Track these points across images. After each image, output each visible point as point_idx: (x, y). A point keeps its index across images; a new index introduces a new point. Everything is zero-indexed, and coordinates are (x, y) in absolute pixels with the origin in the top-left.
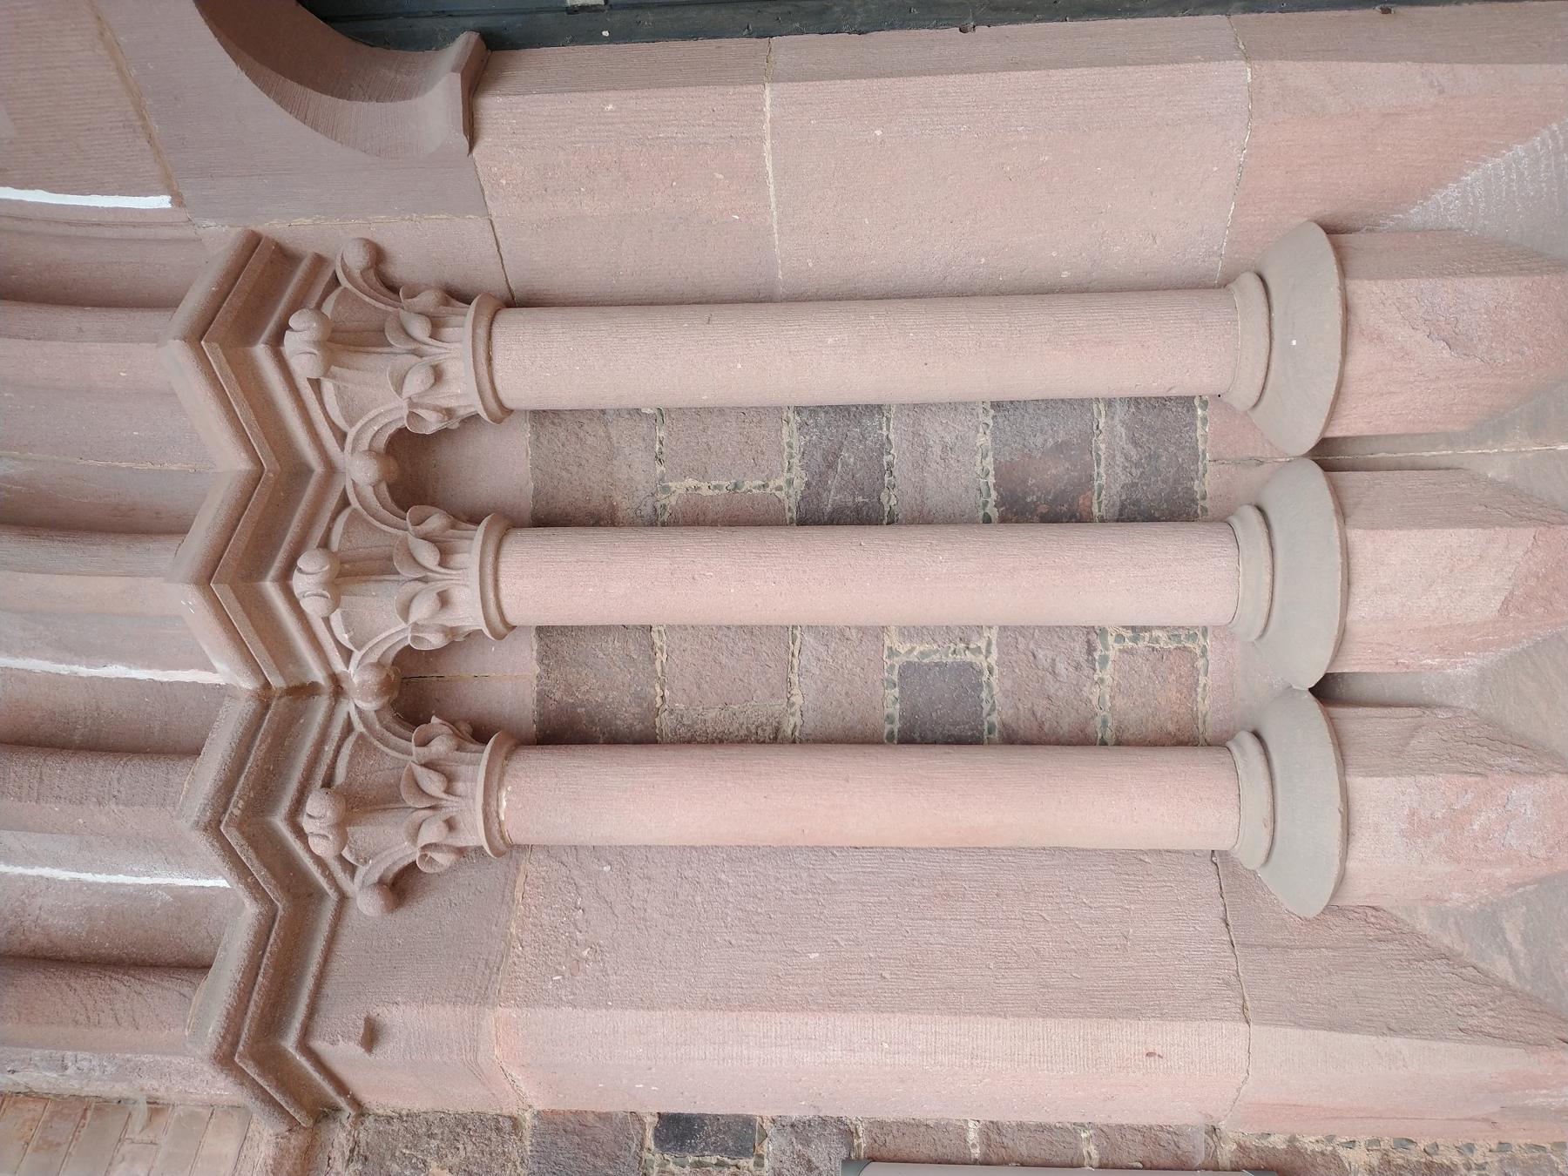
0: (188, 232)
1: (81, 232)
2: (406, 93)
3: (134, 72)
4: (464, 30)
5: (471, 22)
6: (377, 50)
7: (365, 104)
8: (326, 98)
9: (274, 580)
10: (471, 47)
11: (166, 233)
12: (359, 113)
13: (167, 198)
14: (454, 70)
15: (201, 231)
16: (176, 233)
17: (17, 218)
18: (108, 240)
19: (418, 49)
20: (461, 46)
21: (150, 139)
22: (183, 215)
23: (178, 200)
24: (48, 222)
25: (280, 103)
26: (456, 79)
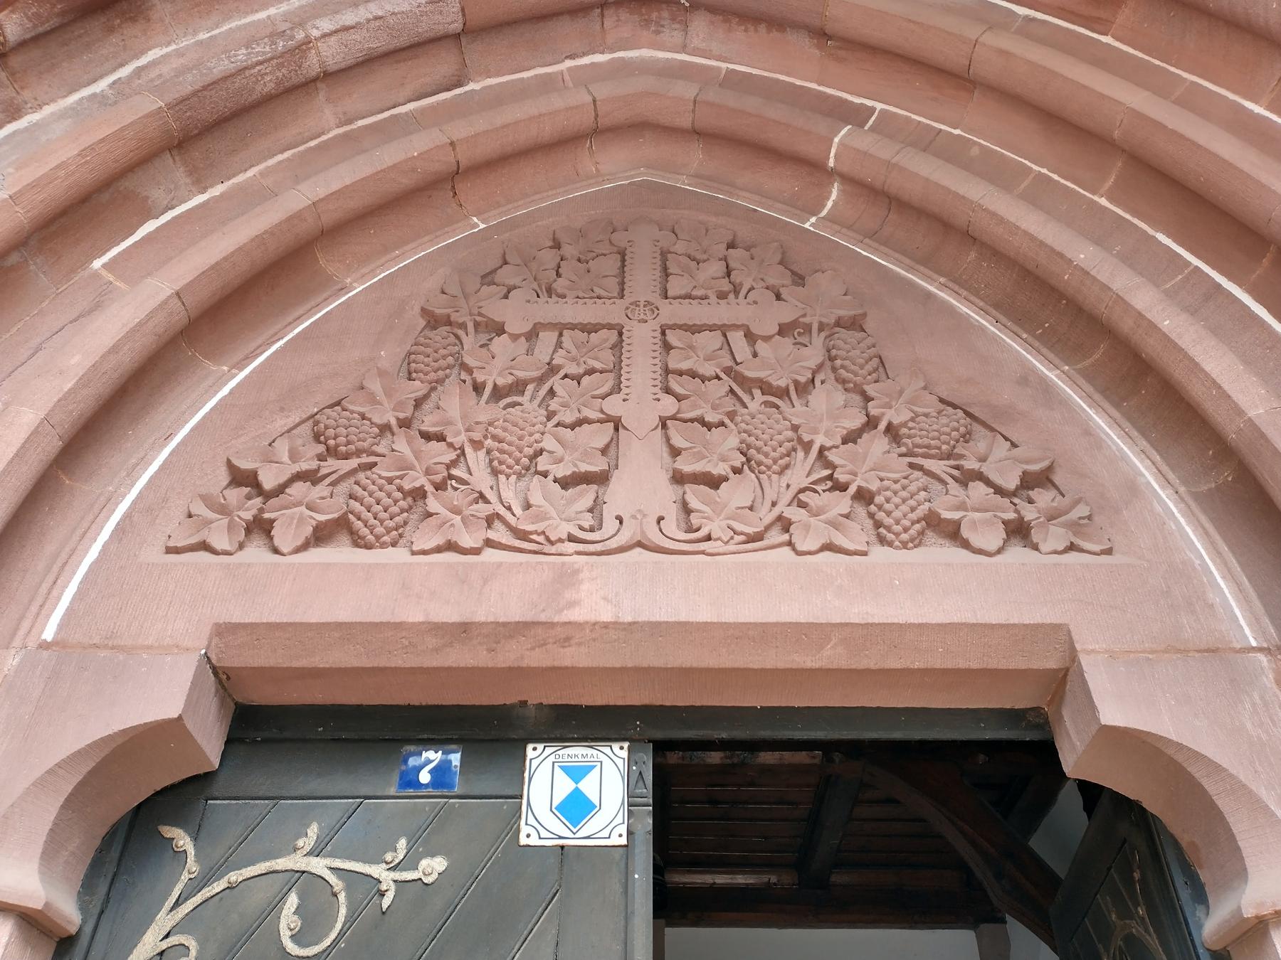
0: (17, 642)
1: (55, 569)
2: (49, 854)
3: (145, 656)
4: (84, 921)
5: (88, 929)
6: (98, 842)
7: (52, 818)
8: (70, 788)
9: (423, 486)
10: (64, 924)
11: (26, 625)
12: (48, 810)
13: (49, 639)
14: (47, 904)
15: (13, 651)
16: (21, 633)
17: (85, 533)
18: (41, 582)
19: (86, 876)
20: (69, 912)
21: (96, 646)
22: (32, 644)
23: (44, 646)
24: (74, 551)
25: (79, 751)
26: (37, 905)
